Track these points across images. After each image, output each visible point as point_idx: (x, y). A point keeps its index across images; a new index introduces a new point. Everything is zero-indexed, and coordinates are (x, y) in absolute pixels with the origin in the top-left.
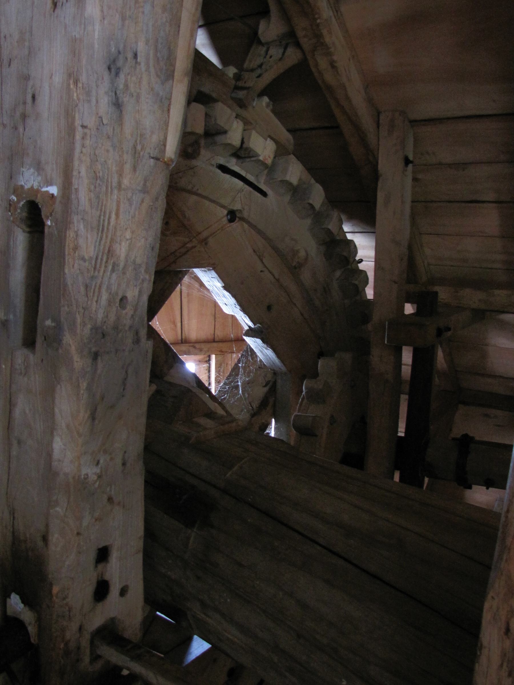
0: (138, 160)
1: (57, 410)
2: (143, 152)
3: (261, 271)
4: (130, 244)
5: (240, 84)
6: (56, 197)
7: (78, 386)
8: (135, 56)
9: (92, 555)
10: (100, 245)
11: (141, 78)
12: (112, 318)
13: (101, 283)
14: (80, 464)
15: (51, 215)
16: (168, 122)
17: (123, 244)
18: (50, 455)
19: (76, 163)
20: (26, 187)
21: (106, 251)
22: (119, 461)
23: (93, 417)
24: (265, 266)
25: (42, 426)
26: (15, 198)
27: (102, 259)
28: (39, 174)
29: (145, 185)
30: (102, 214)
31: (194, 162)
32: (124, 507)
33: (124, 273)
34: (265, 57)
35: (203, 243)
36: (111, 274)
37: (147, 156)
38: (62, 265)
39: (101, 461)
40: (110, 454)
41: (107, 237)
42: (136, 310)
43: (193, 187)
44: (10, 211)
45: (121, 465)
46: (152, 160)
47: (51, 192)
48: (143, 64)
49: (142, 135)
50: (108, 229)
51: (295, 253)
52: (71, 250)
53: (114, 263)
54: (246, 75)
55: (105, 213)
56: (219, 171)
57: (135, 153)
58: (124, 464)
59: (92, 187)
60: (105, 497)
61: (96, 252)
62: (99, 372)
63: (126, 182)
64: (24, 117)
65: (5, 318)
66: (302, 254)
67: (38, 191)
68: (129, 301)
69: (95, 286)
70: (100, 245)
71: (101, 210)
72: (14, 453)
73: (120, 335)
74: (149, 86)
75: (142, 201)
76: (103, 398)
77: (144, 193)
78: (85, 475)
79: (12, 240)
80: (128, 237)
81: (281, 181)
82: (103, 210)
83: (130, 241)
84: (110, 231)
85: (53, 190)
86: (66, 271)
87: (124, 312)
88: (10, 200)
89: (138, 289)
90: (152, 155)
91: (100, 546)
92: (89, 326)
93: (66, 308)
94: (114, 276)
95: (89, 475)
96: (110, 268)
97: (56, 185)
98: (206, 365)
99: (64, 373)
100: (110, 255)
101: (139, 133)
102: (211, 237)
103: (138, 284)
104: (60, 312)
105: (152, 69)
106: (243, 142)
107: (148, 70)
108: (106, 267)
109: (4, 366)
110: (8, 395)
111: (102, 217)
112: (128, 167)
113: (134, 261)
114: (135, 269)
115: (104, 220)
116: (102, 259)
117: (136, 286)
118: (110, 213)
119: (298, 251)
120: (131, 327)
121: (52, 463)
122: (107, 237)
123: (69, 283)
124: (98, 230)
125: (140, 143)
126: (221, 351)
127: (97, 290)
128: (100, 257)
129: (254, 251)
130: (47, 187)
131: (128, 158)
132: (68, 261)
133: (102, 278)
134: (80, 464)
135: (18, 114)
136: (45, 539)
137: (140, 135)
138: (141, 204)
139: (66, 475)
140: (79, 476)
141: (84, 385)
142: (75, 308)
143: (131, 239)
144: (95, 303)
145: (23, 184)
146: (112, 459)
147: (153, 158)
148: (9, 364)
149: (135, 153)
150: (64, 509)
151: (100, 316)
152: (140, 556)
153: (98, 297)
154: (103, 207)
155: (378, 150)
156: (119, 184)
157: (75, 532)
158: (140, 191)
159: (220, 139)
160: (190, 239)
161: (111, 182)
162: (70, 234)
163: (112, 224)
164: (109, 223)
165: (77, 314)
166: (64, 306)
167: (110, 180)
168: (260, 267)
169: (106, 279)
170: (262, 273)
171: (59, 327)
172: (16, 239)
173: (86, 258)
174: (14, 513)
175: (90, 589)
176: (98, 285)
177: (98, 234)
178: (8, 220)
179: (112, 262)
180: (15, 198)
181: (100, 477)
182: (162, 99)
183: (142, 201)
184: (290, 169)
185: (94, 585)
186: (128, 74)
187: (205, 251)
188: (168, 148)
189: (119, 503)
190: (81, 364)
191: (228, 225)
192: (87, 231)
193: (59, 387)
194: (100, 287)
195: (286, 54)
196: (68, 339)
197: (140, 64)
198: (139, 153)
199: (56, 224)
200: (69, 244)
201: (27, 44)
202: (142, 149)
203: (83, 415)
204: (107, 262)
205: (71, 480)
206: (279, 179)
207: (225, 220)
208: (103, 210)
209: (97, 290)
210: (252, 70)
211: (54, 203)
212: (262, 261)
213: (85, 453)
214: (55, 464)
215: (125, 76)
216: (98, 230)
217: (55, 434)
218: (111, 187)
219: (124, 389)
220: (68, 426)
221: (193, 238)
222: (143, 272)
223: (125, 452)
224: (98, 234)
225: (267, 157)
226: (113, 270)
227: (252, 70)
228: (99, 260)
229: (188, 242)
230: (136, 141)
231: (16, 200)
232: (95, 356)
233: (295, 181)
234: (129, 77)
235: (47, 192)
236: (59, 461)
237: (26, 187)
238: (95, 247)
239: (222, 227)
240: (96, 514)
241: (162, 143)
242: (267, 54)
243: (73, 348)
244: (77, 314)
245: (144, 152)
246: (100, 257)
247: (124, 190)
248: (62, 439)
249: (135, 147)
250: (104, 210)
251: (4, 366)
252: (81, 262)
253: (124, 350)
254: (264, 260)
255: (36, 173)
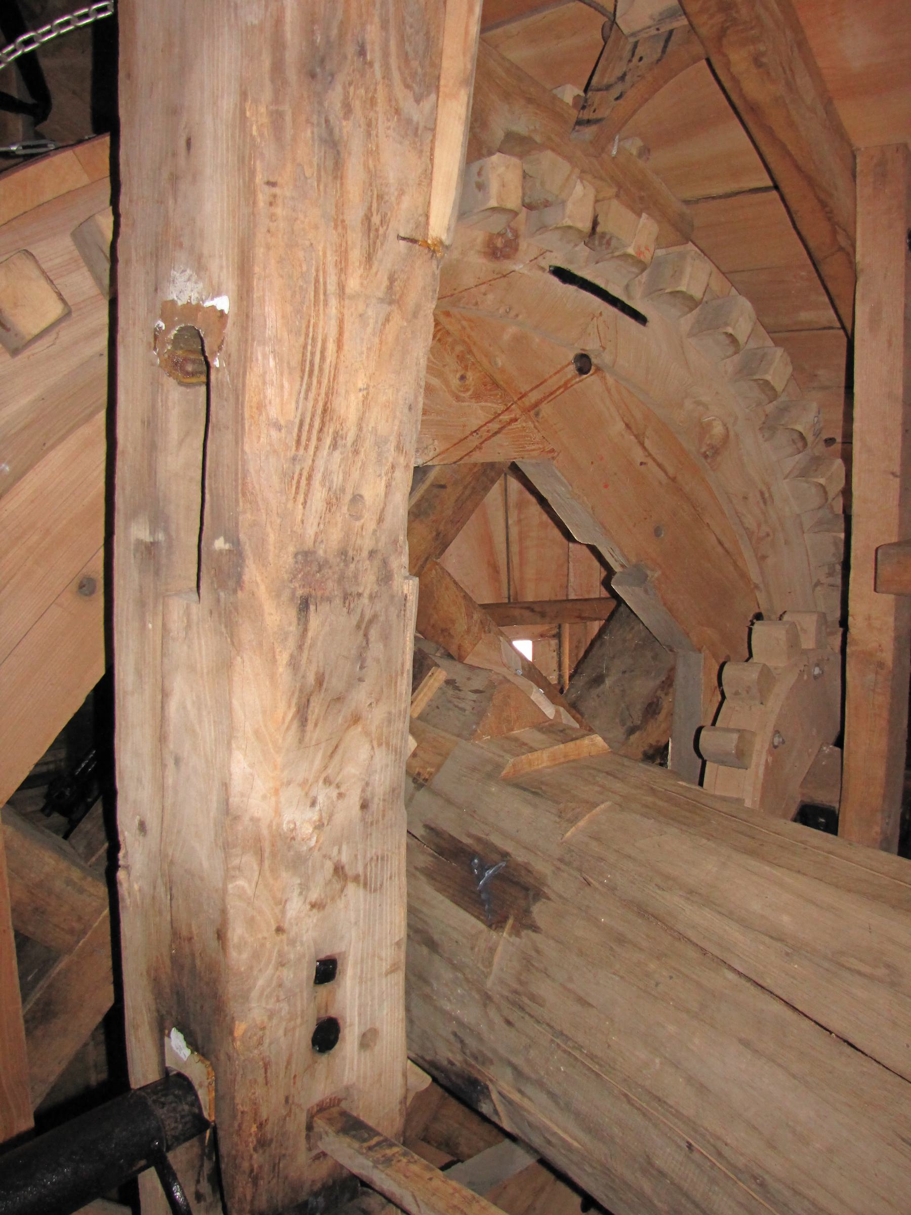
0: (375, 243)
1: (236, 703)
2: (385, 227)
3: (641, 464)
4: (365, 398)
5: (586, 115)
6: (227, 316)
7: (274, 661)
8: (362, 52)
9: (308, 972)
10: (306, 398)
11: (376, 90)
12: (335, 536)
13: (312, 469)
14: (278, 803)
15: (220, 349)
16: (432, 173)
17: (352, 398)
18: (225, 786)
19: (260, 252)
20: (180, 303)
21: (319, 411)
22: (354, 799)
23: (302, 716)
24: (650, 455)
25: (213, 733)
26: (162, 325)
27: (311, 426)
28: (200, 278)
29: (390, 287)
30: (310, 341)
31: (509, 265)
32: (365, 885)
33: (356, 452)
34: (630, 61)
35: (532, 413)
36: (330, 454)
37: (392, 237)
38: (238, 439)
39: (320, 799)
40: (338, 786)
41: (319, 383)
42: (381, 520)
43: (508, 310)
44: (155, 349)
45: (358, 807)
46: (401, 242)
47: (219, 308)
48: (377, 66)
49: (380, 197)
50: (321, 370)
51: (704, 429)
52: (254, 410)
53: (336, 433)
54: (595, 97)
55: (314, 339)
56: (555, 281)
57: (369, 229)
58: (364, 806)
59: (289, 294)
60: (329, 866)
61: (300, 411)
62: (310, 634)
63: (353, 284)
64: (174, 179)
65: (152, 540)
66: (718, 429)
67: (198, 307)
68: (367, 503)
69: (301, 474)
70: (306, 398)
71: (307, 335)
72: (170, 781)
73: (352, 566)
74: (391, 106)
75: (387, 320)
76: (320, 681)
77: (390, 303)
78: (289, 822)
79: (159, 401)
80: (360, 385)
81: (671, 293)
82: (311, 335)
83: (365, 392)
84: (326, 371)
85: (223, 303)
86: (247, 448)
87: (358, 524)
88: (155, 330)
89: (383, 483)
90: (402, 235)
91: (322, 956)
92: (291, 549)
93: (249, 516)
94: (337, 455)
95: (298, 824)
96: (328, 441)
97: (227, 294)
98: (554, 642)
99: (246, 633)
100: (328, 418)
101: (375, 193)
102: (546, 402)
103: (383, 472)
104: (237, 523)
105: (396, 75)
106: (595, 223)
107: (387, 76)
108: (319, 439)
109: (150, 626)
110: (159, 677)
111: (309, 348)
112: (356, 255)
113: (375, 429)
114: (377, 444)
115: (313, 354)
116: (311, 426)
117: (380, 475)
118: (324, 342)
119: (709, 424)
120: (372, 553)
121: (231, 800)
122: (319, 383)
123: (252, 470)
124: (303, 371)
125: (378, 211)
126: (580, 617)
127: (303, 482)
128: (308, 421)
129: (628, 426)
130: (212, 299)
131: (356, 239)
132: (249, 429)
133: (313, 461)
134: (278, 803)
135: (165, 175)
136: (221, 935)
137: (378, 196)
138: (384, 325)
139: (255, 820)
140: (279, 825)
141: (283, 658)
142: (264, 516)
143: (367, 389)
144: (301, 507)
145: (176, 298)
146: (340, 795)
147: (404, 239)
148: (160, 623)
149: (369, 229)
150: (254, 885)
151: (311, 531)
152: (399, 978)
153: (306, 495)
154: (311, 329)
155: (855, 223)
156: (341, 287)
157: (274, 928)
158: (381, 300)
159: (551, 217)
160: (505, 405)
161: (325, 283)
162: (252, 380)
163: (328, 361)
164: (323, 358)
165: (268, 525)
166: (245, 512)
167: (321, 280)
168: (638, 455)
169: (320, 464)
170: (643, 467)
171: (237, 553)
172: (167, 397)
173: (282, 422)
174: (171, 889)
175: (305, 1032)
176: (305, 474)
177: (302, 378)
178: (153, 365)
179: (331, 431)
180: (162, 325)
181: (319, 826)
182: (417, 129)
183: (387, 320)
184: (688, 270)
185: (312, 1027)
186: (350, 84)
187: (535, 427)
188: (433, 220)
189: (356, 879)
190: (278, 619)
191: (577, 380)
192: (282, 374)
193: (239, 658)
194: (310, 478)
195: (668, 50)
196: (252, 572)
197: (371, 64)
198: (377, 230)
199: (228, 364)
200: (251, 398)
201: (176, 50)
202: (382, 223)
203: (285, 711)
204: (321, 430)
205: (265, 832)
206: (668, 290)
207: (572, 370)
208: (311, 335)
209: (303, 482)
210: (608, 87)
211: (224, 325)
212: (642, 444)
213: (289, 783)
214: (234, 800)
215: (344, 88)
216: (303, 371)
217: (234, 745)
218: (325, 294)
219: (362, 668)
220: (257, 733)
221: (512, 404)
222: (392, 449)
223: (367, 784)
224: (302, 378)
225: (643, 249)
226: (334, 446)
227: (608, 87)
228: (306, 427)
229: (503, 412)
230: (370, 208)
231: (164, 328)
232: (304, 606)
233: (697, 292)
234: (352, 89)
235: (213, 307)
236: (242, 795)
237: (180, 303)
238: (297, 402)
239: (566, 384)
240: (314, 896)
241: (420, 211)
242: (633, 55)
243: (262, 588)
244: (268, 525)
245: (387, 229)
246: (308, 421)
247: (352, 297)
248: (245, 755)
249: (368, 218)
250: (313, 335)
251: (150, 626)
252: (274, 433)
253: (359, 595)
254: (647, 443)
255: (195, 277)
